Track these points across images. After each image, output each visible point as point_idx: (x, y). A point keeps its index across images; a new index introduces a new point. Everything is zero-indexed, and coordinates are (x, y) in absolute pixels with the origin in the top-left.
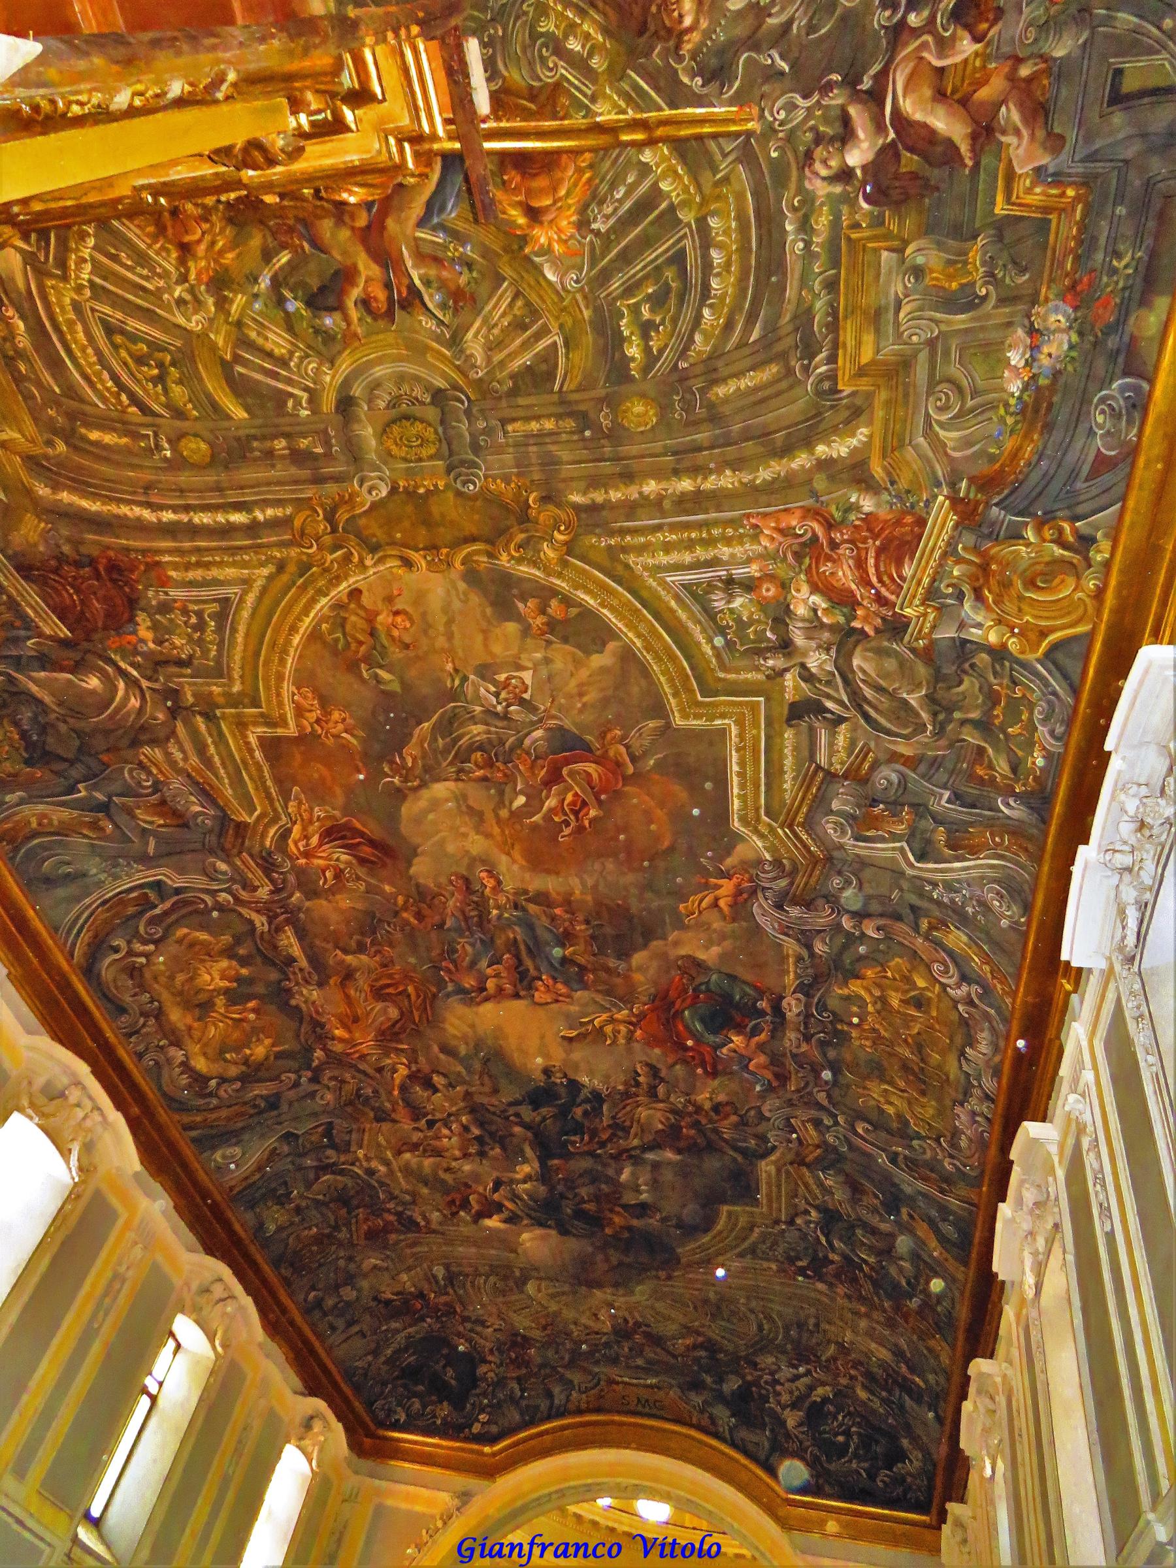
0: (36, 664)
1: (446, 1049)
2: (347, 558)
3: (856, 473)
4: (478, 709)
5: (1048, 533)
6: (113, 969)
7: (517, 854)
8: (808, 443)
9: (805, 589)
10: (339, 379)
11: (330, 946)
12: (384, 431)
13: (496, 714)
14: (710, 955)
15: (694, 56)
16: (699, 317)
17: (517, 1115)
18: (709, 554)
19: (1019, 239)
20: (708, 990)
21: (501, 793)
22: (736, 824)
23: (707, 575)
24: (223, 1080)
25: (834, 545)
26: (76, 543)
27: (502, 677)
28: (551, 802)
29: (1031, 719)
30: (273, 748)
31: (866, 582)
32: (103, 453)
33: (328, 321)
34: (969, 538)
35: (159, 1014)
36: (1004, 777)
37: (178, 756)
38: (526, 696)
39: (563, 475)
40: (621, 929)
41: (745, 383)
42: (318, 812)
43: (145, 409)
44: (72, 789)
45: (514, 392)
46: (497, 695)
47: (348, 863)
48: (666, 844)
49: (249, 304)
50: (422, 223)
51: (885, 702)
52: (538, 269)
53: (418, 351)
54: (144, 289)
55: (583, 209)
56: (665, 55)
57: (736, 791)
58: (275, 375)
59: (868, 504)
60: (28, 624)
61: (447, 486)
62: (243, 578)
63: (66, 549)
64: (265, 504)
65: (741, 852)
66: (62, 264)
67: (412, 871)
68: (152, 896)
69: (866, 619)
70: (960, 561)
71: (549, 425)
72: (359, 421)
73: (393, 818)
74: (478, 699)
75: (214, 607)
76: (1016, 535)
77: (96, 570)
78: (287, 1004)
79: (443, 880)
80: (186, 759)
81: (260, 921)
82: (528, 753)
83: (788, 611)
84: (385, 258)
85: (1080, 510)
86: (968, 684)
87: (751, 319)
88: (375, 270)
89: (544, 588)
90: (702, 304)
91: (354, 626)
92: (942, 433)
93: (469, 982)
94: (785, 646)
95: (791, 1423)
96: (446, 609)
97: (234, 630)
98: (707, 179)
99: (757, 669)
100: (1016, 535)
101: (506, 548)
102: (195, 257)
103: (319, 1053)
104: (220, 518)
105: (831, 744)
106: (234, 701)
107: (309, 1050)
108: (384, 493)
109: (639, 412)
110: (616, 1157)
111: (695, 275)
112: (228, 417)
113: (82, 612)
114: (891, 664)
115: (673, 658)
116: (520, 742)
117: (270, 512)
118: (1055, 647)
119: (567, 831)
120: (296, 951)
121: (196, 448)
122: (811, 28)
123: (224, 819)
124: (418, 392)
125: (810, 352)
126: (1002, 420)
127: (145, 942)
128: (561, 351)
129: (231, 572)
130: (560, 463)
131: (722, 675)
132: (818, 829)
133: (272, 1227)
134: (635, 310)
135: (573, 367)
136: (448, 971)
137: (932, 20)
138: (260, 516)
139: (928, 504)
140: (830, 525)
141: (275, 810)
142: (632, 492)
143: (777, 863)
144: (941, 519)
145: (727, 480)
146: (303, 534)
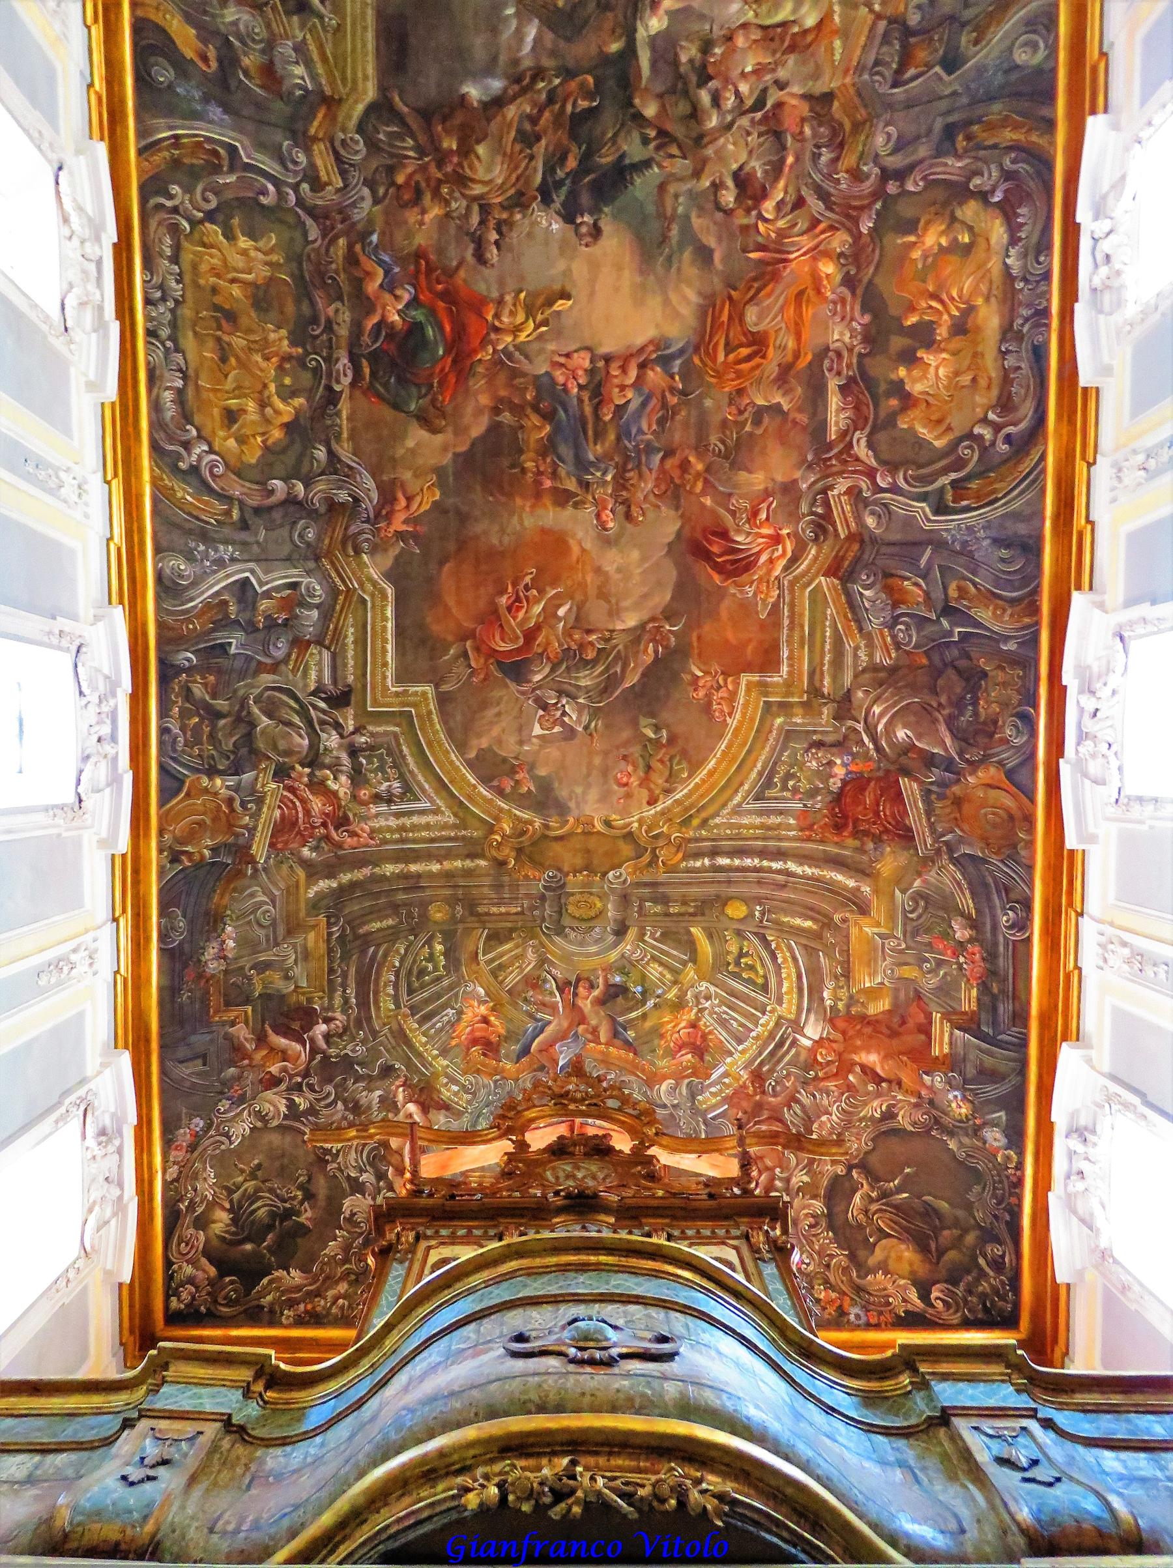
0: (937, 761)
3: (313, 871)
5: (197, 857)
7: (576, 550)
8: (342, 890)
9: (341, 794)
10: (620, 948)
12: (601, 913)
13: (568, 696)
14: (416, 436)
16: (402, 961)
19: (236, 996)
22: (390, 591)
23: (405, 807)
25: (324, 825)
26: (861, 850)
27: (557, 729)
28: (537, 609)
29: (185, 734)
30: (768, 660)
31: (303, 801)
32: (809, 911)
33: (618, 979)
34: (241, 841)
36: (195, 682)
37: (862, 654)
38: (541, 712)
41: (378, 925)
44: (964, 637)
46: (564, 713)
47: (739, 531)
48: (447, 567)
50: (550, 1022)
52: (487, 994)
53: (567, 958)
55: (459, 1020)
57: (389, 625)
58: (662, 952)
59: (306, 852)
60: (927, 794)
61: (567, 875)
62: (740, 817)
65: (387, 560)
66: (778, 1025)
67: (678, 524)
70: (245, 827)
71: (494, 910)
74: (580, 709)
76: (214, 850)
77: (855, 827)
78: (875, 317)
79: (651, 515)
80: (857, 648)
82: (548, 658)
85: (181, 876)
86: (229, 744)
88: (580, 1003)
89: (514, 801)
91: (661, 774)
92: (265, 899)
93: (655, 376)
94: (353, 752)
97: (760, 774)
98: (395, 1027)
99: (372, 735)
100: (214, 850)
101: (535, 830)
104: (737, 862)
105: (320, 672)
106: (785, 707)
108: (611, 874)
109: (438, 914)
112: (704, 929)
114: (282, 745)
116: (553, 670)
117: (698, 864)
118: (179, 790)
119: (528, 579)
120: (834, 401)
121: (736, 910)
124: (573, 935)
125: (342, 938)
128: (480, 951)
129: (745, 821)
131: (397, 729)
134: (436, 969)
138: (707, 861)
139: (268, 857)
140: (327, 838)
141: (792, 591)
142: (447, 865)
143: (358, 551)
144: (260, 849)
145: (389, 869)
146: (679, 848)
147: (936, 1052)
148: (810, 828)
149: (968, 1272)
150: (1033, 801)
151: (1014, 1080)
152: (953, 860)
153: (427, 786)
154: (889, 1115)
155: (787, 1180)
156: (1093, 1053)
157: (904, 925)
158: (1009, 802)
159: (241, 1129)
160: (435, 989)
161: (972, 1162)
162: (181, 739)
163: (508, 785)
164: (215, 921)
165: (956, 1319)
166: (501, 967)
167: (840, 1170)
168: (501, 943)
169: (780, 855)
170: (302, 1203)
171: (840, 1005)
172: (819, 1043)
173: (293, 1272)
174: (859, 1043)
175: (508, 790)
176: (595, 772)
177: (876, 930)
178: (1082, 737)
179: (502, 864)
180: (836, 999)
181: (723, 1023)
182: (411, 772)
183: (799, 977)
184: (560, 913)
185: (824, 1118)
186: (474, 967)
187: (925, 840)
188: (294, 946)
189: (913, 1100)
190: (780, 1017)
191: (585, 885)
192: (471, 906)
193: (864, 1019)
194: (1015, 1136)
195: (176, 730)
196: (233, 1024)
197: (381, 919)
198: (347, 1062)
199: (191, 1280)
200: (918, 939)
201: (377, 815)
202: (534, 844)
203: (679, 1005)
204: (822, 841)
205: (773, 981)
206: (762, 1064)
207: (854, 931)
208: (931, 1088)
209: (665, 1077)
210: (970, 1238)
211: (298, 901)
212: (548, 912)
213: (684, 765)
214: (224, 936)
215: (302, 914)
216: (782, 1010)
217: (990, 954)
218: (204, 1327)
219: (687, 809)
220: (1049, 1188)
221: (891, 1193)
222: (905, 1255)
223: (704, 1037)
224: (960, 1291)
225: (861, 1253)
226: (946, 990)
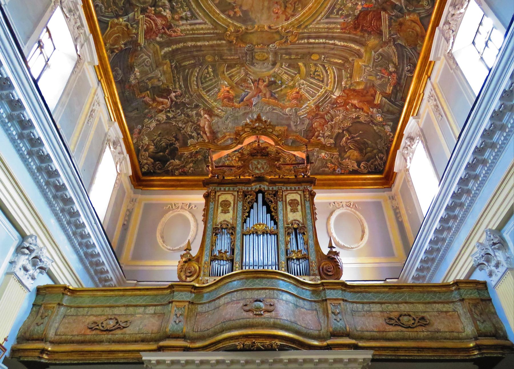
2: (286, 29)
3: (162, 45)
9: (168, 16)
10: (274, 70)
16: (198, 74)
18: (192, 27)
19: (143, 89)
25: (163, 28)
26: (363, 37)
31: (154, 20)
32: (340, 57)
33: (273, 79)
34: (134, 39)
41: (188, 63)
45: (235, 64)
50: (249, 92)
52: (228, 84)
55: (219, 92)
58: (288, 71)
59: (158, 39)
60: (390, 19)
61: (255, 46)
62: (320, 24)
63: (366, 35)
64: (304, 43)
66: (326, 92)
69: (151, 11)
70: (134, 34)
75: (333, 16)
76: (125, 44)
77: (362, 28)
83: (171, 11)
87: (188, 73)
88: (260, 86)
89: (234, 20)
92: (147, 57)
97: (329, 8)
100: (125, 44)
101: (243, 30)
104: (317, 41)
109: (209, 59)
112: (303, 63)
117: (303, 42)
118: (108, 26)
121: (315, 57)
125: (176, 67)
129: (321, 26)
130: (227, 50)
135: (224, 67)
138: (306, 41)
140: (165, 33)
144: (141, 40)
145: (189, 44)
147: (376, 102)
148: (345, 29)
149: (373, 158)
150: (426, 31)
151: (397, 115)
152: (394, 44)
153: (200, 14)
154: (358, 117)
155: (324, 134)
156: (420, 120)
157: (373, 63)
158: (418, 29)
159: (154, 124)
160: (210, 83)
161: (380, 133)
162: (103, 7)
163: (232, 14)
164: (131, 68)
165: (366, 171)
166: (233, 76)
167: (340, 131)
168: (232, 68)
169: (333, 38)
170: (175, 141)
171: (347, 86)
172: (339, 97)
173: (176, 161)
174: (352, 97)
175: (232, 15)
176: (265, 8)
177: (363, 64)
178: (447, 22)
179: (231, 42)
180: (346, 84)
181: (307, 92)
182: (194, 9)
183: (335, 78)
184: (253, 59)
186: (223, 76)
187: (386, 35)
188: (160, 71)
190: (327, 90)
191: (261, 49)
192: (221, 56)
193: (354, 90)
194: (394, 129)
195: (100, 5)
196: (144, 97)
197: (189, 60)
198: (184, 104)
199: (147, 164)
200: (377, 68)
201: (183, 25)
202: (242, 35)
203: (293, 87)
204: (349, 33)
205: (326, 79)
206: (319, 103)
207: (356, 64)
209: (287, 107)
210: (375, 151)
211: (158, 56)
212: (248, 58)
213: (300, 5)
214: (135, 72)
215: (161, 60)
216: (328, 88)
217: (399, 77)
218: (153, 176)
219: (300, 22)
221: (355, 137)
222: (356, 154)
223: (301, 96)
224: (369, 164)
225: (343, 154)
226: (383, 86)
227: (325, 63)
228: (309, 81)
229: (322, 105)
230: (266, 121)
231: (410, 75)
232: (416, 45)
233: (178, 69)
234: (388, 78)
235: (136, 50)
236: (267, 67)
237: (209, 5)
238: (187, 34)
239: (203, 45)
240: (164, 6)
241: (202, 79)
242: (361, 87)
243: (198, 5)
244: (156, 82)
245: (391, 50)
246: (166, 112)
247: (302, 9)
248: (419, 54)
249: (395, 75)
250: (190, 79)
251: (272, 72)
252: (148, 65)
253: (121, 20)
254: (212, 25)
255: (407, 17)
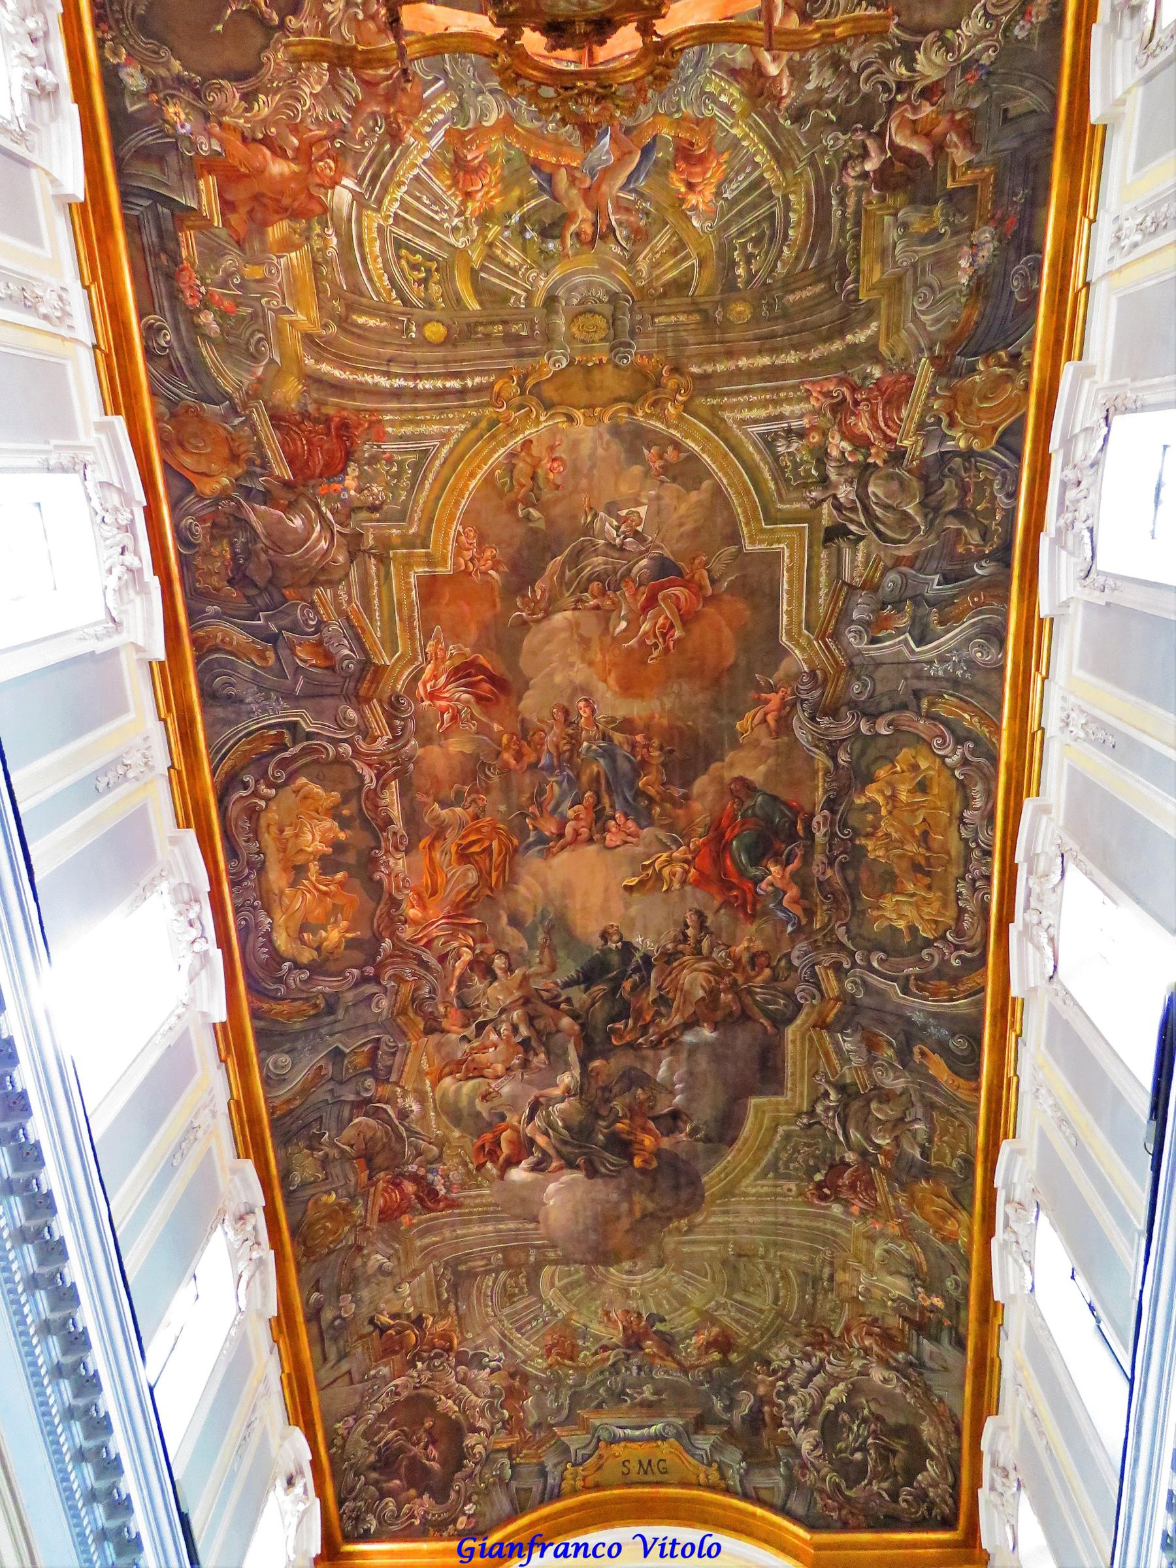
1: (515, 921)
3: (871, 352)
4: (602, 542)
5: (992, 361)
6: (239, 806)
7: (612, 680)
8: (842, 333)
9: (838, 437)
10: (551, 282)
11: (429, 800)
14: (757, 775)
15: (787, 109)
17: (568, 1000)
20: (754, 815)
21: (607, 621)
24: (297, 966)
25: (856, 403)
26: (320, 404)
27: (623, 513)
28: (645, 627)
30: (430, 588)
32: (362, 334)
33: (551, 246)
34: (943, 381)
35: (261, 868)
36: (976, 546)
38: (639, 529)
39: (687, 353)
40: (689, 753)
41: (806, 293)
42: (452, 650)
43: (406, 302)
44: (254, 616)
45: (664, 295)
46: (617, 529)
49: (501, 233)
50: (622, 188)
51: (890, 517)
52: (689, 218)
53: (607, 268)
54: (432, 219)
55: (719, 186)
56: (772, 107)
59: (877, 372)
60: (265, 464)
62: (441, 431)
63: (311, 408)
64: (473, 374)
66: (380, 201)
68: (287, 738)
69: (877, 455)
70: (938, 397)
72: (557, 313)
73: (515, 649)
75: (411, 458)
76: (972, 370)
77: (329, 428)
79: (546, 714)
80: (349, 601)
81: (369, 774)
83: (827, 454)
84: (597, 209)
85: (1009, 340)
88: (589, 215)
89: (664, 437)
90: (783, 244)
92: (923, 318)
94: (824, 481)
95: (806, 1447)
96: (592, 456)
97: (425, 477)
99: (804, 499)
100: (972, 370)
101: (642, 407)
102: (474, 200)
103: (387, 944)
104: (439, 384)
107: (378, 939)
109: (741, 310)
110: (656, 1046)
111: (779, 226)
113: (307, 461)
115: (748, 492)
116: (630, 570)
117: (478, 380)
118: (1001, 437)
119: (655, 654)
120: (396, 812)
121: (435, 331)
122: (847, 101)
123: (366, 664)
124: (600, 294)
126: (959, 301)
127: (269, 786)
128: (696, 269)
131: (779, 506)
132: (845, 643)
133: (298, 1180)
134: (744, 246)
135: (701, 283)
136: (535, 818)
137: (909, 97)
138: (469, 383)
140: (854, 389)
141: (414, 650)
142: (730, 365)
143: (813, 674)
144: (925, 371)
145: (792, 358)
154: (249, 98)
156: (51, 191)
158: (187, 461)
163: (670, 453)
164: (978, 289)
166: (674, 252)
167: (293, 22)
169: (397, 394)
172: (334, 183)
175: (670, 449)
177: (293, 317)
178: (130, 528)
180: (323, 237)
185: (318, 89)
189: (226, 119)
192: (707, 320)
193: (295, 215)
195: (1000, 496)
196: (970, 165)
198: (843, 124)
201: (802, 416)
203: (485, 218)
204: (358, 411)
206: (392, 153)
207: (315, 314)
208: (210, 135)
209: (492, 128)
212: (627, 319)
213: (499, 483)
214: (970, 271)
215: (884, 304)
217: (176, 298)
219: (493, 437)
220: (65, 16)
223: (455, 183)
226: (213, 253)
227: (403, 314)
228: (441, 244)
229: (381, 144)
230: (564, 121)
231: (151, 319)
232: (173, 415)
233: (837, 270)
234: (206, 285)
235: (947, 345)
236: (570, 290)
237: (726, 474)
238: (795, 388)
239: (754, 356)
240: (843, 464)
241: (771, 233)
242: (277, 231)
243: (753, 471)
244: (915, 219)
245: (232, 378)
246: (911, 84)
247: (491, 473)
248: (153, 393)
249: (190, 302)
250: (807, 230)
251: (556, 274)
252: (924, 290)
253: (962, 444)
254: (723, 420)
255: (225, 481)
